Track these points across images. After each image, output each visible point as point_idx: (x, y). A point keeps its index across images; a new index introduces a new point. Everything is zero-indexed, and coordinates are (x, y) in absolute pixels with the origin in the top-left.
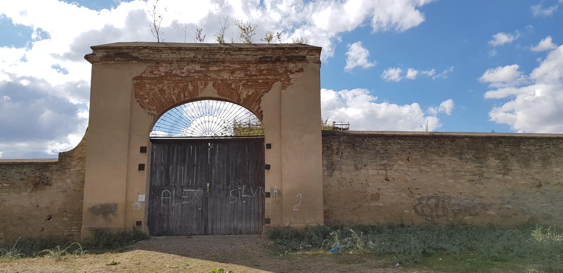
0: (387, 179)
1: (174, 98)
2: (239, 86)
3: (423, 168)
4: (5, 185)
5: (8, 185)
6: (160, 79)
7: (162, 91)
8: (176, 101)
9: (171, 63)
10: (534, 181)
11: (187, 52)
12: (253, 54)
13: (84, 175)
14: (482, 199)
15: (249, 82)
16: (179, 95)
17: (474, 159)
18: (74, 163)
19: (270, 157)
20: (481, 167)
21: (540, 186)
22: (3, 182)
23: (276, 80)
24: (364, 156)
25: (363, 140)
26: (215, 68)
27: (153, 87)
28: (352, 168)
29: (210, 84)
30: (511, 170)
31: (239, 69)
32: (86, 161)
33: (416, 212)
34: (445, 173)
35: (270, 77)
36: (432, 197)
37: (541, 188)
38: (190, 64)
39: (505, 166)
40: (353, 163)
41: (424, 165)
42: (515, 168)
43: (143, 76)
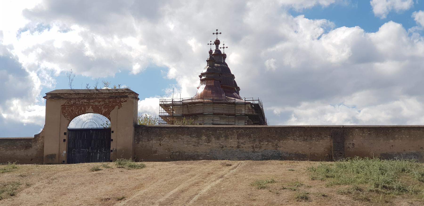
0: (160, 145)
1: (77, 113)
2: (102, 108)
3: (175, 140)
4: (15, 147)
5: (16, 147)
6: (71, 106)
7: (72, 110)
8: (77, 114)
9: (75, 99)
10: (220, 145)
11: (82, 95)
12: (107, 95)
13: (44, 143)
14: (198, 153)
15: (106, 106)
16: (78, 112)
17: (196, 136)
18: (40, 139)
19: (113, 136)
20: (199, 140)
21: (223, 147)
22: (14, 146)
23: (116, 105)
24: (152, 135)
25: (152, 129)
26: (92, 101)
27: (69, 109)
28: (147, 140)
29: (91, 107)
30: (211, 141)
31: (102, 101)
32: (17, 164)
33: (171, 158)
34: (184, 142)
35: (114, 104)
36: (177, 152)
37: (223, 148)
38: (83, 99)
39: (209, 140)
40: (147, 138)
41: (175, 139)
42: (213, 140)
43: (65, 104)
